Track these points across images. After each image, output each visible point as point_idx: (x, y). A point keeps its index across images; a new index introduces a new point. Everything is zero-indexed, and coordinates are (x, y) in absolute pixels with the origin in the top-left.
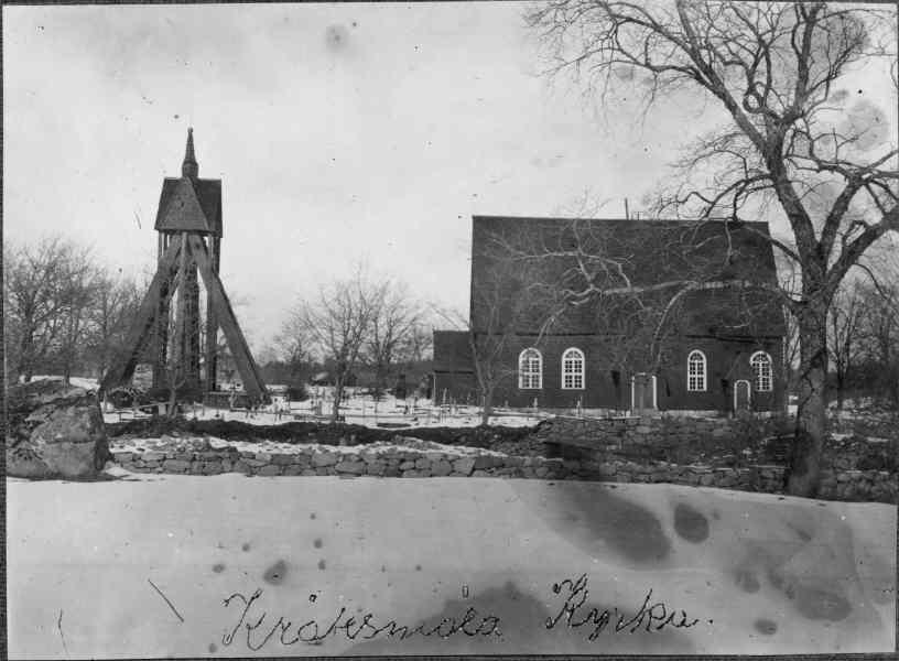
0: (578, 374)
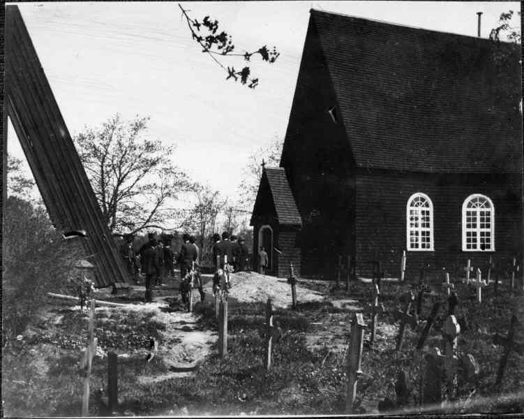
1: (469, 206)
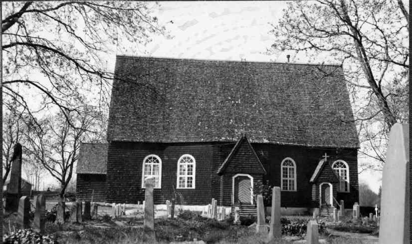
0: (285, 179)
1: (284, 165)
